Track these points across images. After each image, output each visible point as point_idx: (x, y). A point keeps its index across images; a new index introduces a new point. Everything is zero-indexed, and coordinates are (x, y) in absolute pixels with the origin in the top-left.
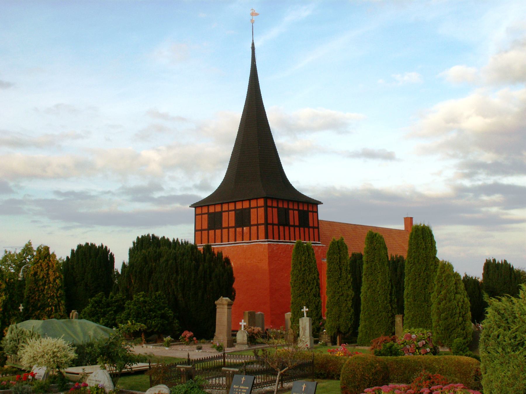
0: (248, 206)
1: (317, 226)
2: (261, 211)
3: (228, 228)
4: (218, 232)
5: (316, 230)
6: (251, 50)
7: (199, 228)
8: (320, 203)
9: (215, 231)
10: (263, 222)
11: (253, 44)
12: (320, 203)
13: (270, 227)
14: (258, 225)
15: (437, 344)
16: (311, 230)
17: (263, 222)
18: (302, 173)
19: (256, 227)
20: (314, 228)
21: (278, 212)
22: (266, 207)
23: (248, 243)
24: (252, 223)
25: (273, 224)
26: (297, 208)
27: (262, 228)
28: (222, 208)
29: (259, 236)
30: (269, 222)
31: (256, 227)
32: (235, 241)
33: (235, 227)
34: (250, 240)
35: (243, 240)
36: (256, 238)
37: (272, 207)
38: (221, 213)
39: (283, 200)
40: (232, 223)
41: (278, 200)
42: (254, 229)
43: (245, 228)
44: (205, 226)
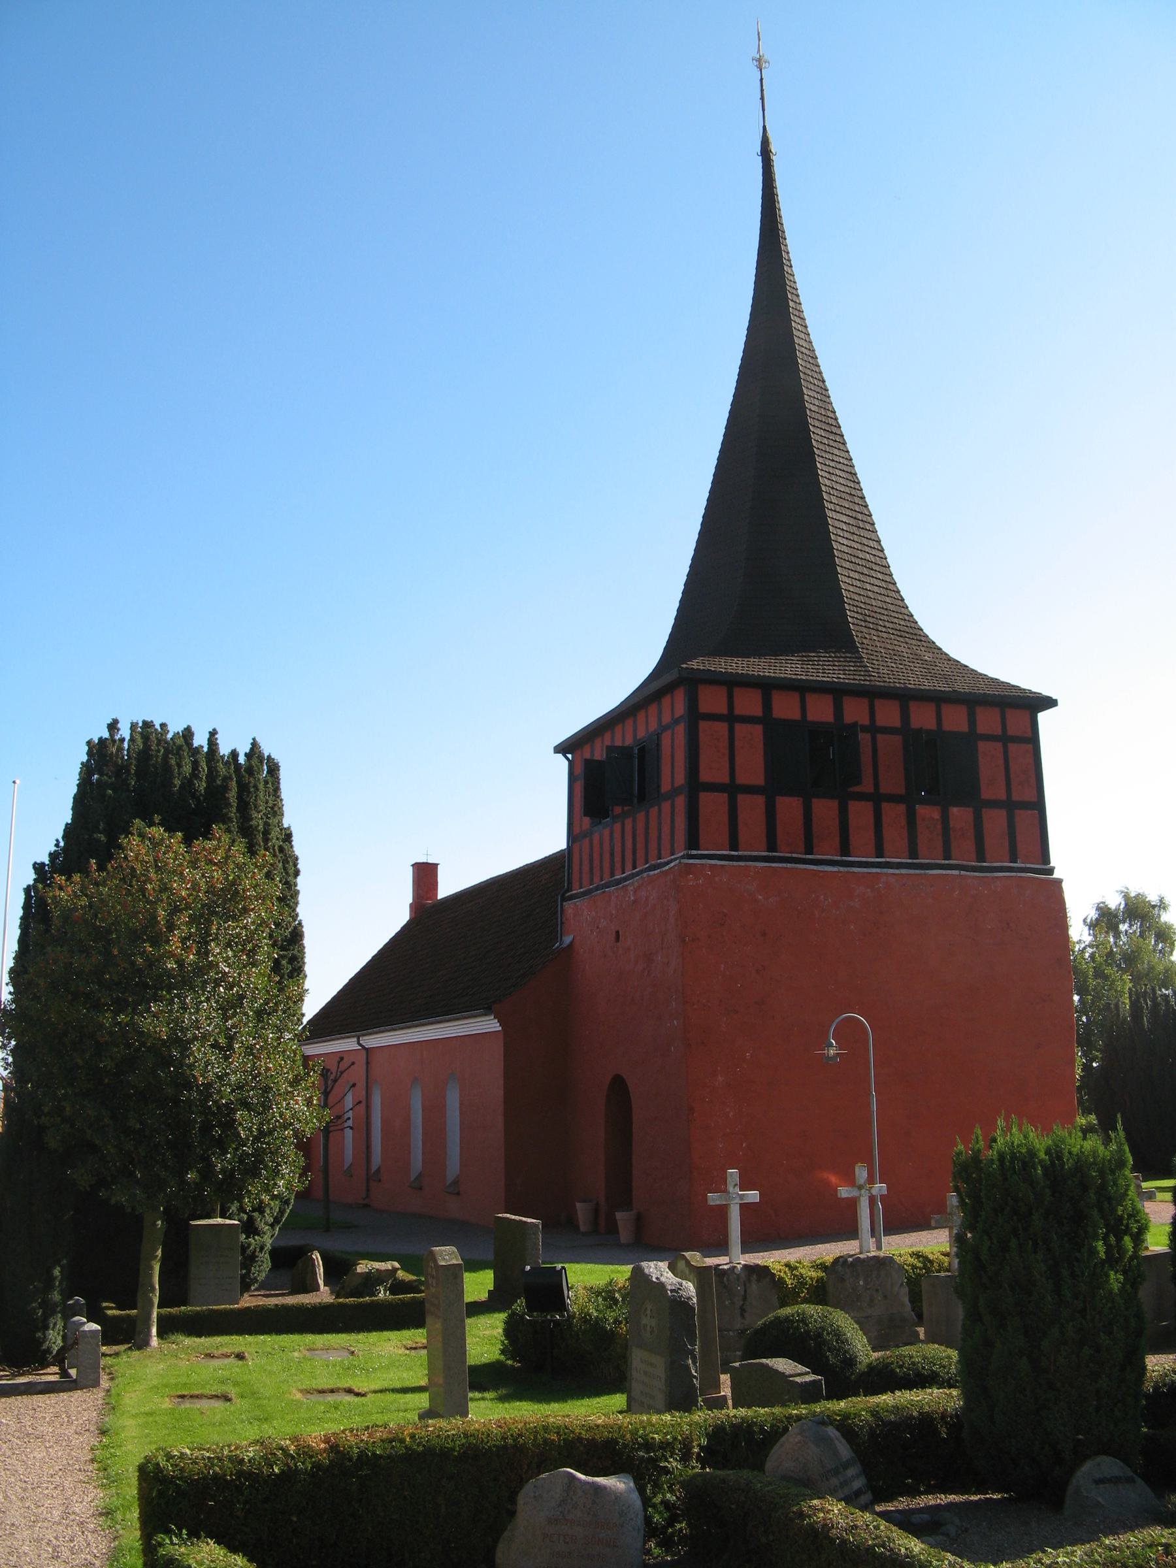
0: (758, 730)
3: (675, 791)
5: (1022, 816)
6: (758, 162)
7: (1022, 816)
8: (1050, 703)
11: (765, 142)
12: (1050, 703)
13: (713, 806)
16: (861, 813)
18: (963, 578)
20: (1010, 806)
23: (974, 869)
25: (733, 790)
26: (758, 711)
27: (681, 802)
30: (705, 776)
31: (1003, 813)
32: (845, 851)
34: (880, 854)
43: (954, 810)
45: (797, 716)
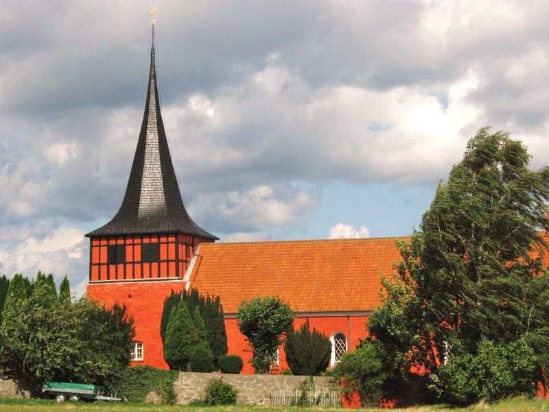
1: (93, 267)
2: (172, 247)
3: (168, 261)
4: (121, 266)
9: (117, 267)
10: (174, 259)
12: (40, 272)
14: (168, 261)
15: (344, 383)
16: (163, 265)
17: (174, 259)
19: (166, 263)
21: (142, 251)
22: (177, 243)
24: (162, 259)
27: (172, 266)
28: (125, 242)
29: (102, 277)
31: (166, 263)
32: (125, 278)
33: (142, 263)
34: (99, 279)
35: (117, 278)
36: (140, 276)
37: (182, 243)
38: (158, 245)
39: (150, 235)
40: (138, 258)
41: (142, 236)
42: (163, 265)
44: (104, 259)
45: (174, 245)
